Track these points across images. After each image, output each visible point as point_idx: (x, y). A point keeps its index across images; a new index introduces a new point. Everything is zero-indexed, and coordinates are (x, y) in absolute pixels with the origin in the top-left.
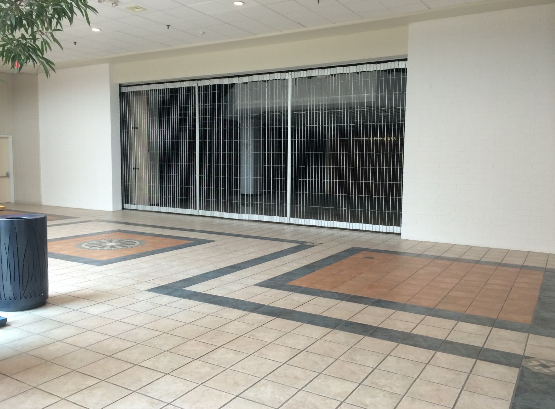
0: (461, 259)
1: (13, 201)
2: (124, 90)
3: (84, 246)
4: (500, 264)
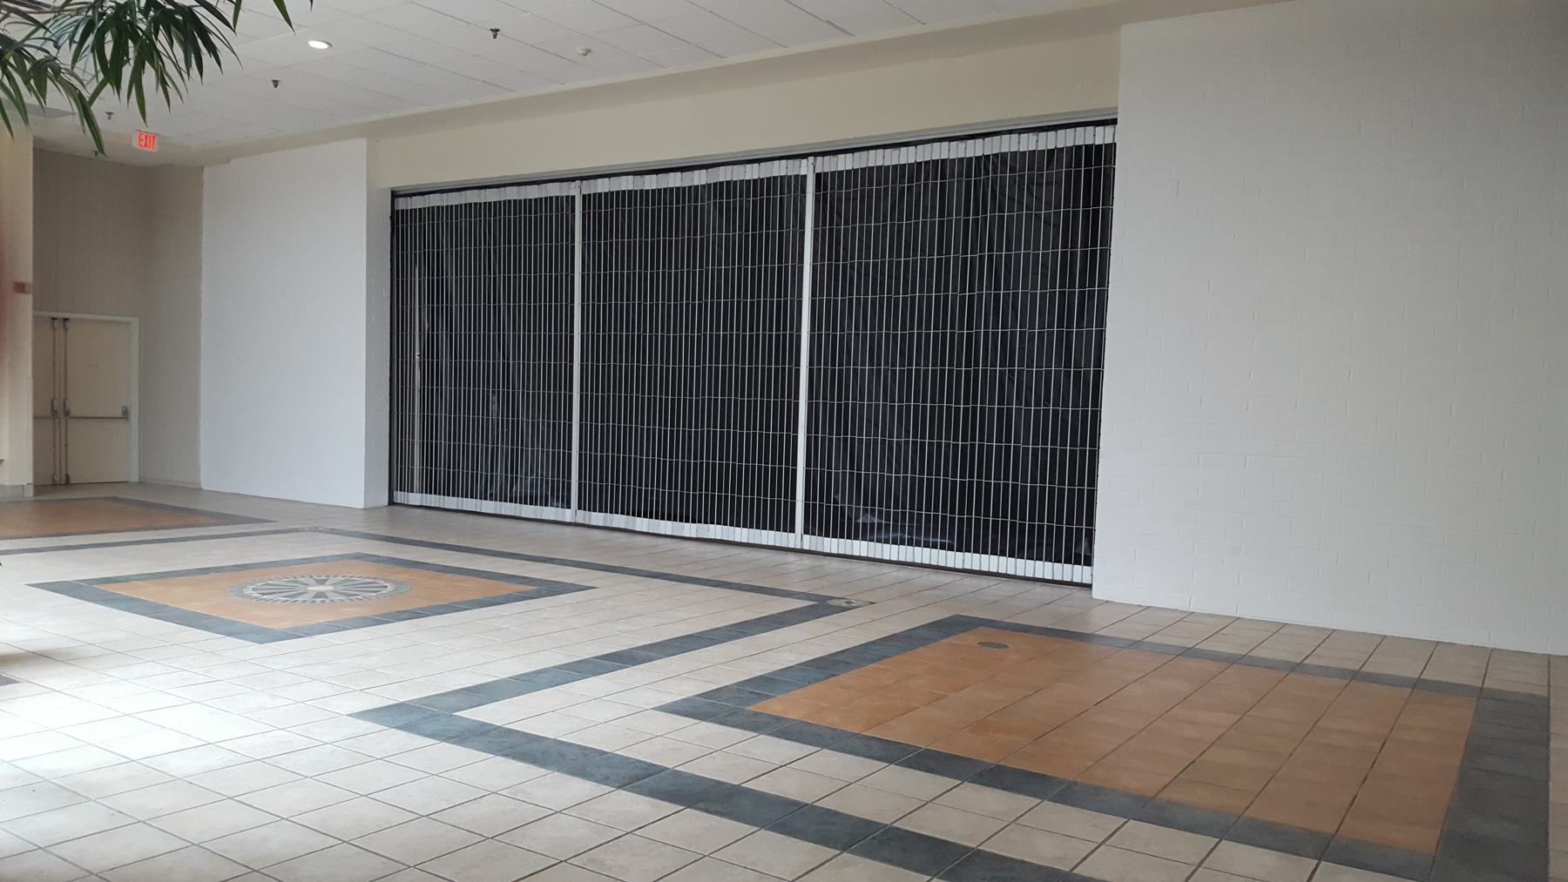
0: (1252, 658)
1: (135, 478)
2: (402, 204)
3: (248, 591)
4: (1355, 675)
